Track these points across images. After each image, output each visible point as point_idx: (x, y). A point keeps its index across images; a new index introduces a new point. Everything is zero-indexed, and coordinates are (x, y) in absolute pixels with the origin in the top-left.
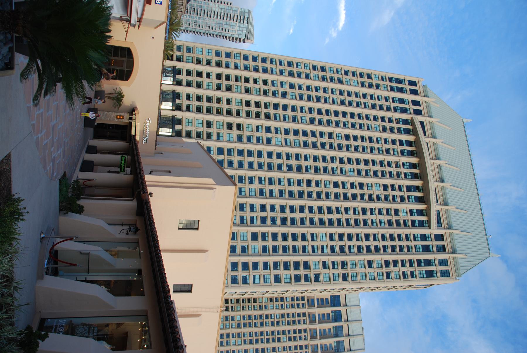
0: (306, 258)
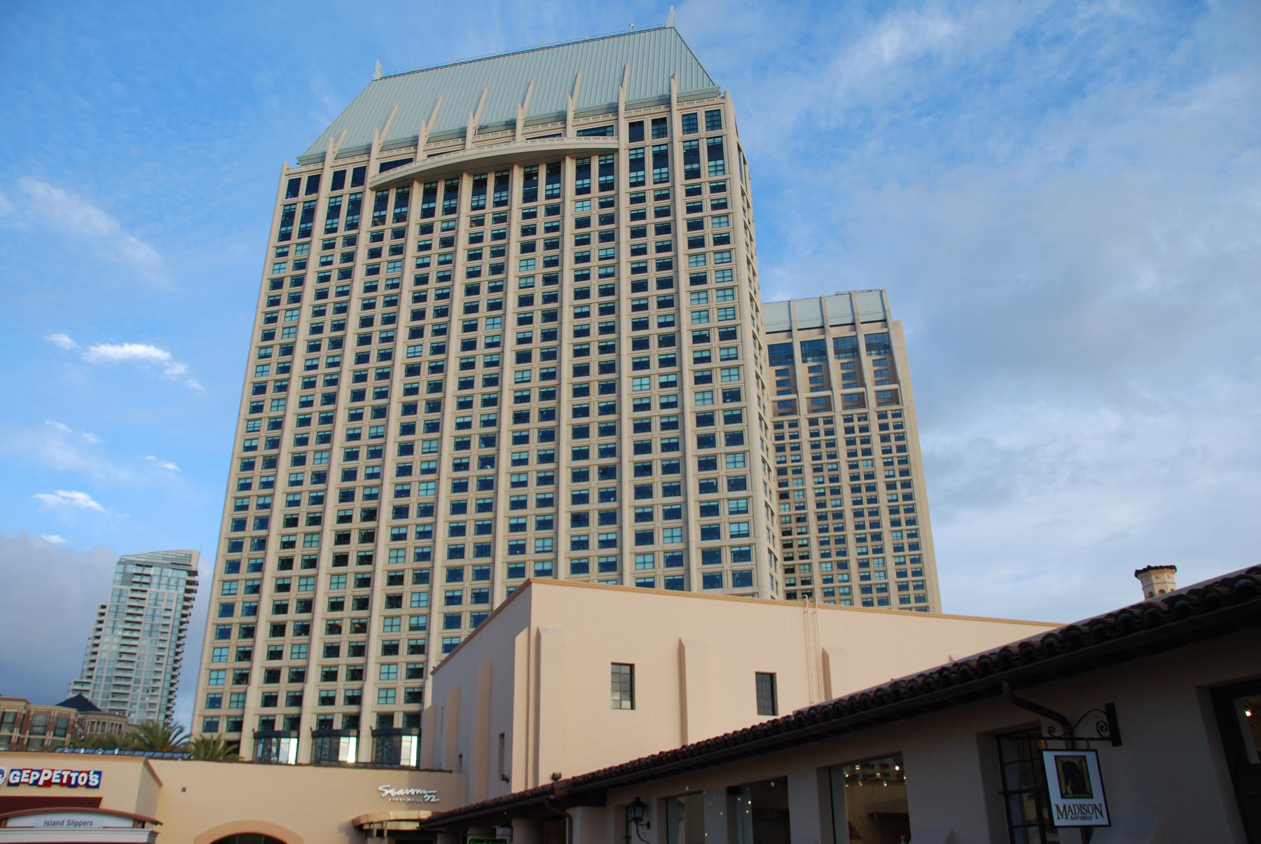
0: (686, 339)
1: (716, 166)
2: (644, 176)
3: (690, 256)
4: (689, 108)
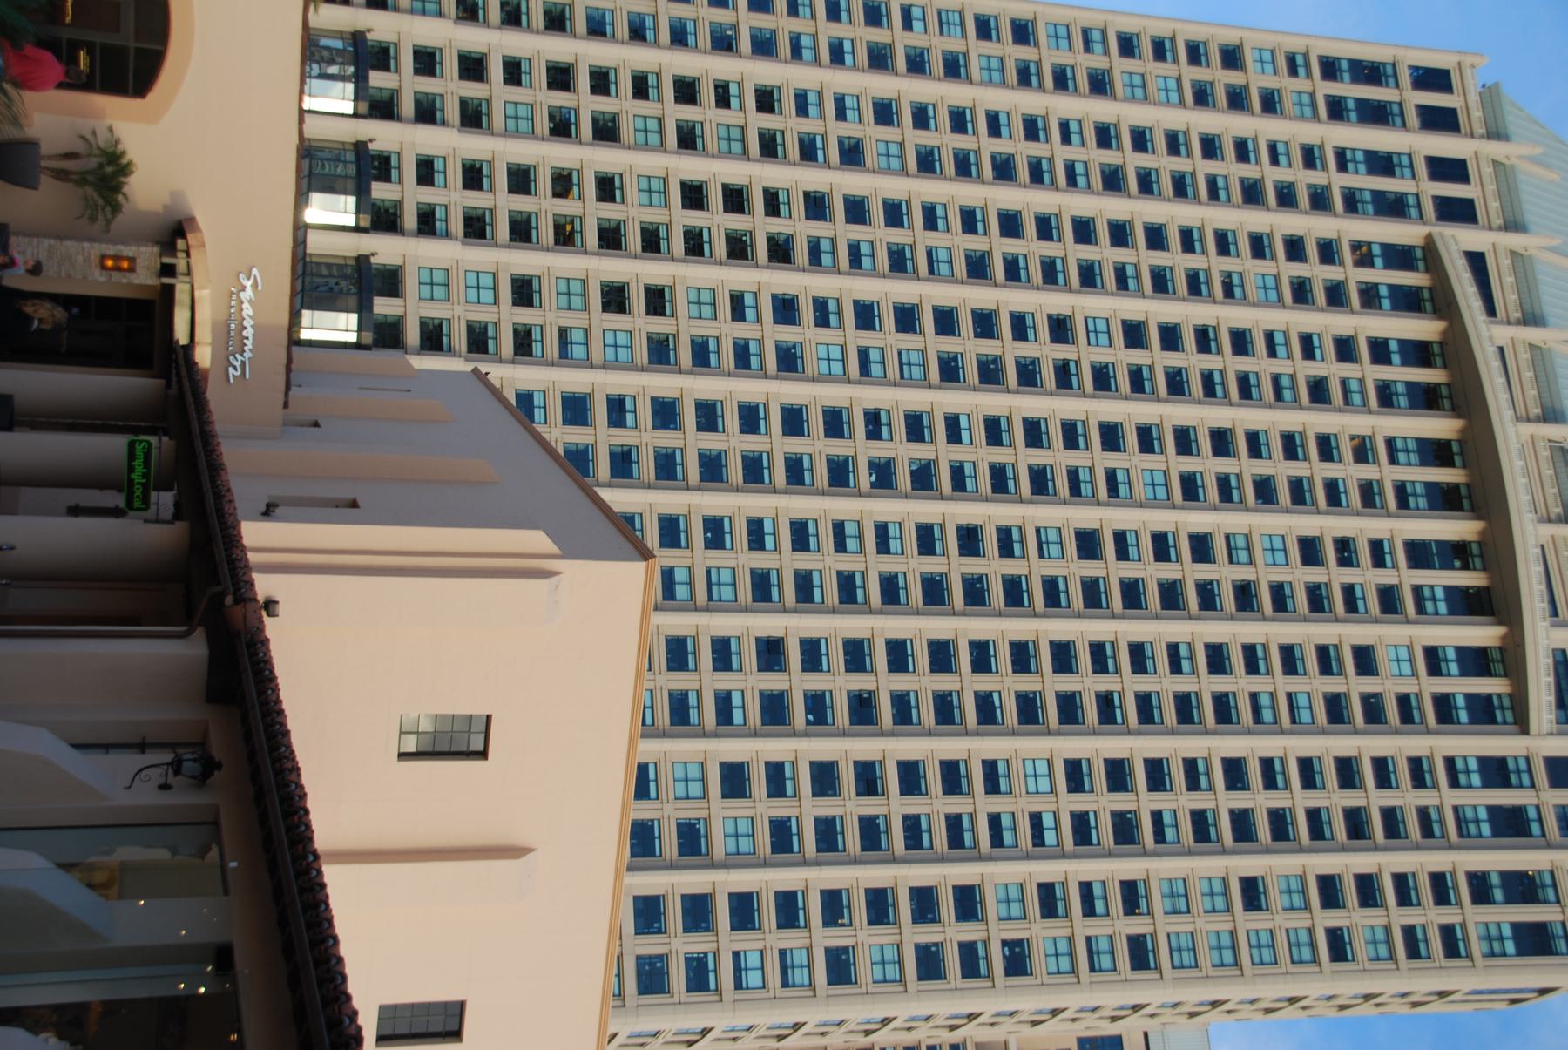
3: (1225, 881)
4: (1481, 172)
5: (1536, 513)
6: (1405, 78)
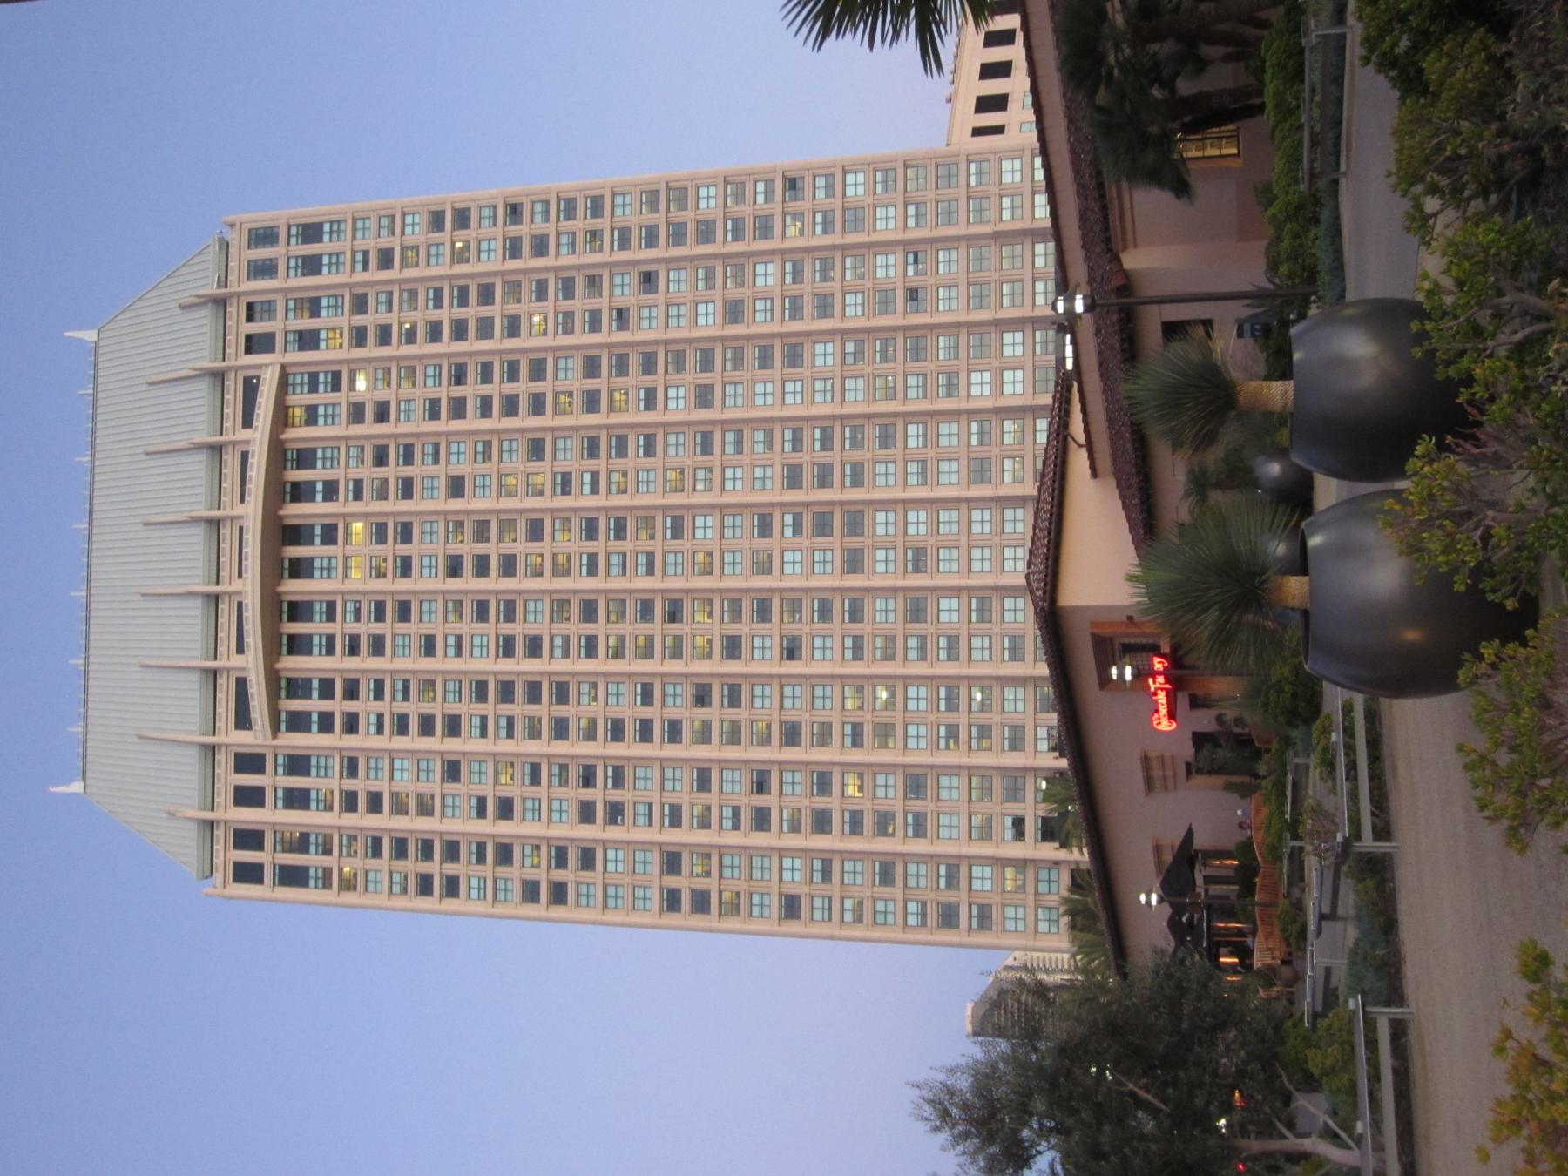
0: (507, 665)
1: (326, 416)
2: (320, 636)
4: (225, 795)
5: (241, 529)
6: (268, 873)
